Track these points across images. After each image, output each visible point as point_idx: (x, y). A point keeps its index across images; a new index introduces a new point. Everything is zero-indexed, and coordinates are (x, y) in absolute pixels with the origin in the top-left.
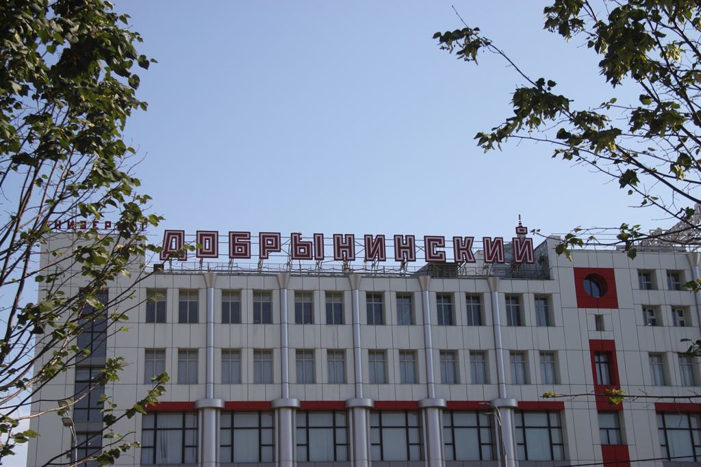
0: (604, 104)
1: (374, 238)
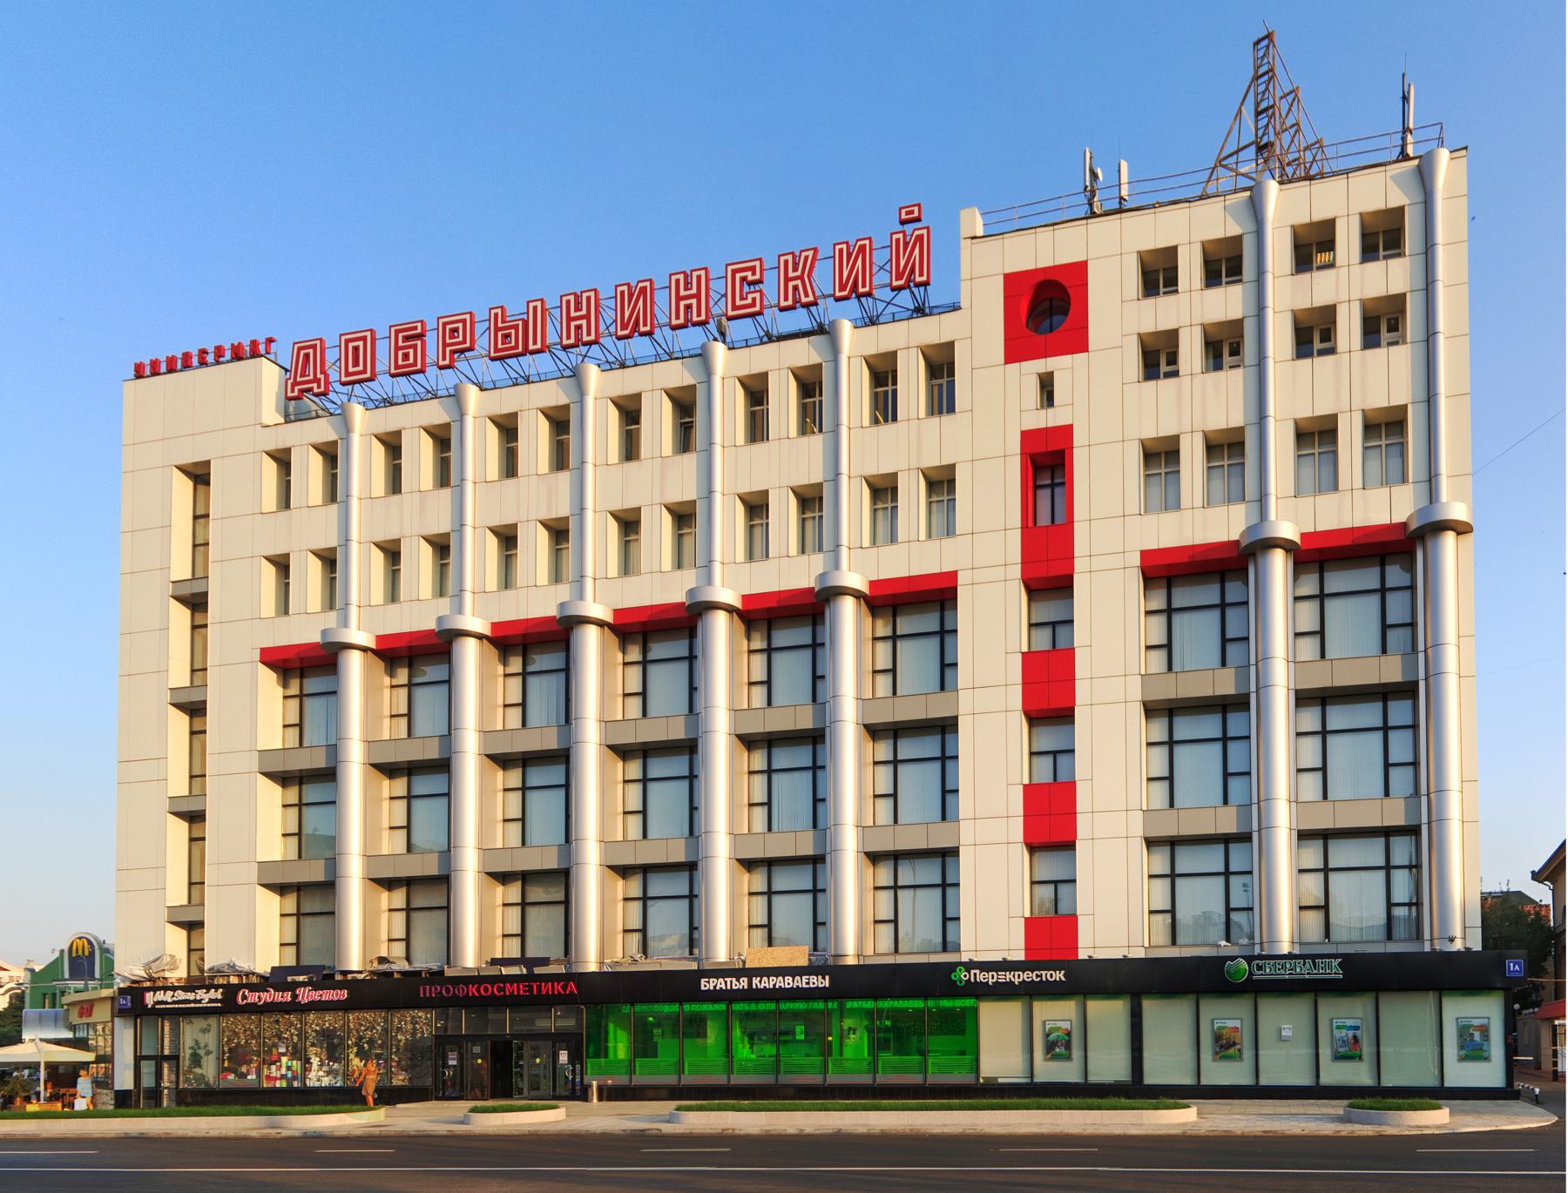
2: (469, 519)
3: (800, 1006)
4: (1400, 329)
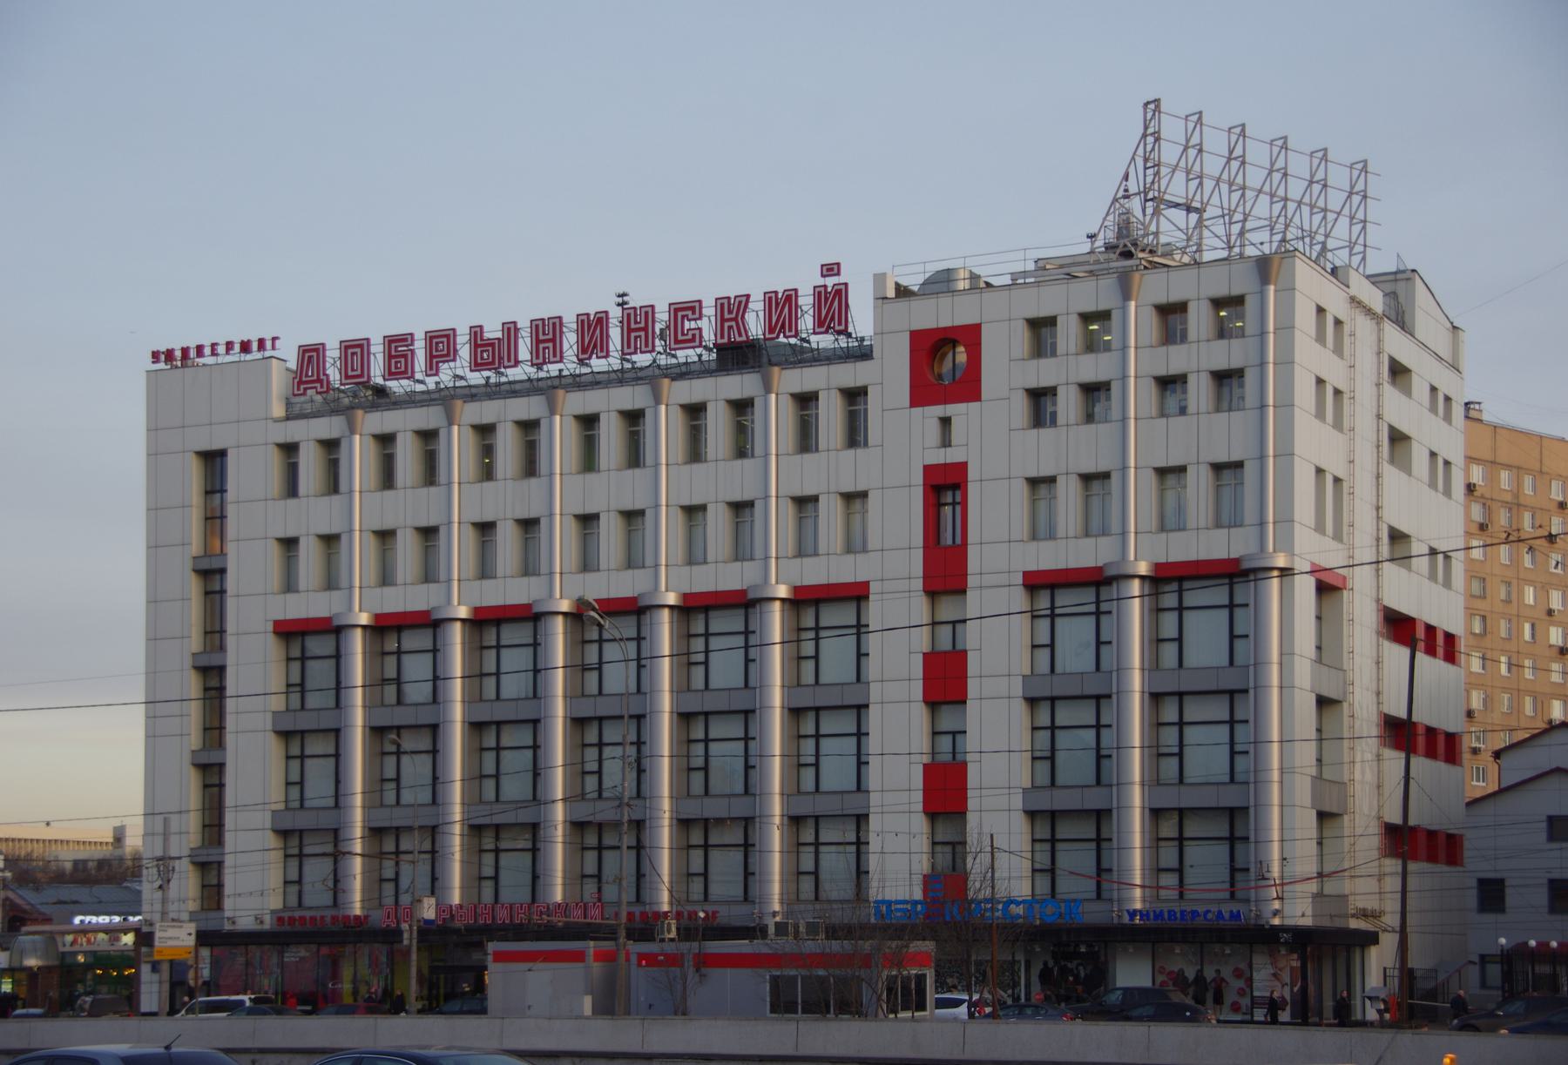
1: (592, 318)
3: (902, 906)
4: (773, 1015)
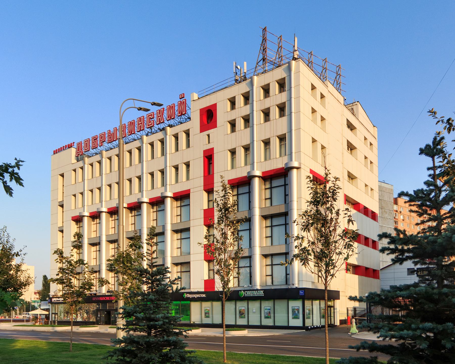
0: (348, 222)
2: (168, 165)
